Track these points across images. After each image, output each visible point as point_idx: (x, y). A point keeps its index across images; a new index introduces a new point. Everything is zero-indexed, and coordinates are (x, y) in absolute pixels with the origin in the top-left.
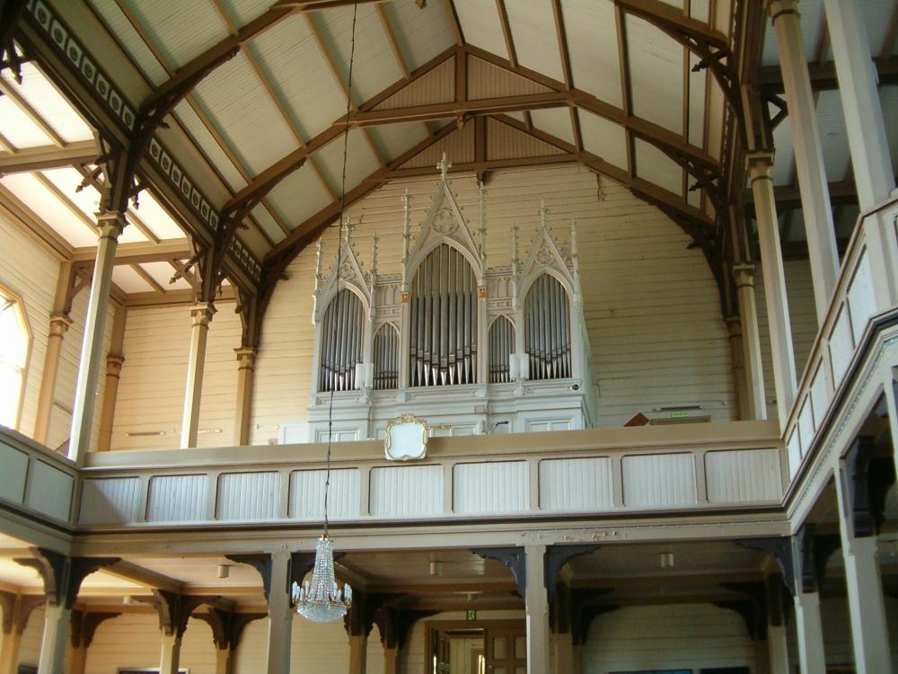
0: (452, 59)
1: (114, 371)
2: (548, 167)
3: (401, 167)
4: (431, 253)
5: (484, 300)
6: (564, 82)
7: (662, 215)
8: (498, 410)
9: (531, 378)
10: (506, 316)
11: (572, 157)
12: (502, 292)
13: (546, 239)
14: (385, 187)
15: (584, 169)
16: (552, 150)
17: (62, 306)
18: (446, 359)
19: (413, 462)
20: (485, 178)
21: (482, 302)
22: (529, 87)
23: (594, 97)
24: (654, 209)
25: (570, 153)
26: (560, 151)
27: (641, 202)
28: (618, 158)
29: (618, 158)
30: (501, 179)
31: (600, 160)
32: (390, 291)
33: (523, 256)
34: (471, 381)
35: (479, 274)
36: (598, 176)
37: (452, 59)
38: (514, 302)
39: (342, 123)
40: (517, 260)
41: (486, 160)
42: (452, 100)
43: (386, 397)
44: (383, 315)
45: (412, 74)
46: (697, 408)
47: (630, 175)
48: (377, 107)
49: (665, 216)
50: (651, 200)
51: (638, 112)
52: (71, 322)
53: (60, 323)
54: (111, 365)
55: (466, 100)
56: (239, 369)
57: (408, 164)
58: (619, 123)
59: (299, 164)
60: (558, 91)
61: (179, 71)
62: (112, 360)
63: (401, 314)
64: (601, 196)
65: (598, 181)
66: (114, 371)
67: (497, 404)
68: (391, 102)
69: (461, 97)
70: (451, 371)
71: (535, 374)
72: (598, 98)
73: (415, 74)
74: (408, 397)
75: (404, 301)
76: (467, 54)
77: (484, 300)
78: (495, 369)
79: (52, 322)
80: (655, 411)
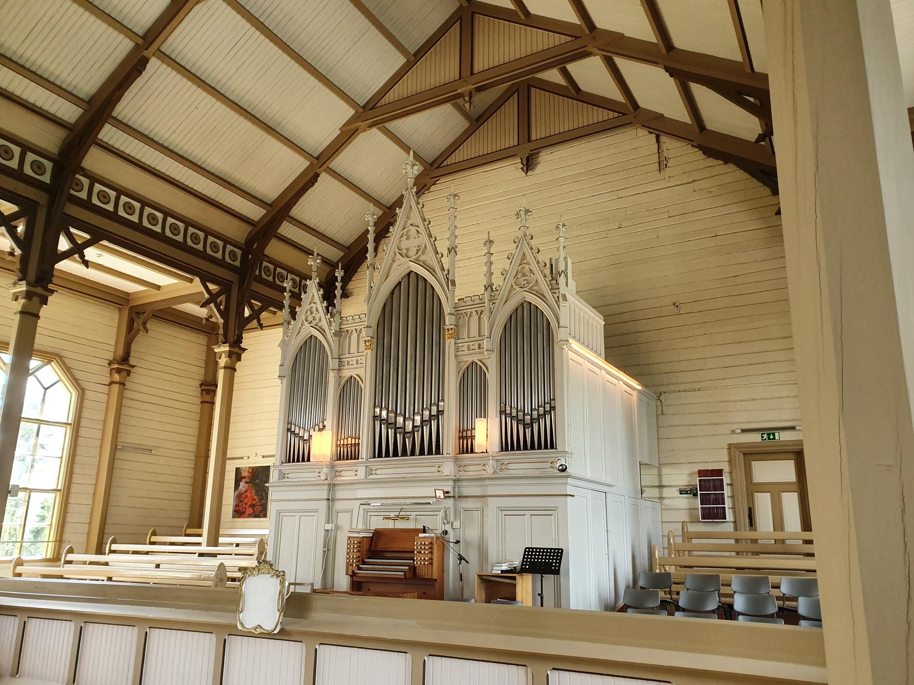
0: (458, 24)
1: (208, 398)
2: (561, 147)
3: (445, 163)
4: (400, 282)
5: (452, 341)
6: (656, 41)
7: (741, 175)
8: (466, 491)
9: (502, 450)
10: (479, 363)
11: (626, 119)
12: (474, 332)
13: (527, 254)
14: (433, 188)
15: (642, 132)
16: (603, 115)
17: (120, 352)
18: (436, 408)
19: (269, 636)
20: (529, 164)
21: (450, 343)
22: (543, 41)
23: (623, 34)
24: (731, 167)
25: (624, 114)
26: (612, 115)
27: (712, 162)
28: (678, 112)
29: (678, 112)
30: (548, 160)
31: (660, 117)
32: (355, 335)
33: (497, 281)
34: (438, 452)
35: (447, 309)
36: (658, 137)
37: (458, 24)
38: (486, 344)
39: (348, 128)
40: (491, 286)
41: (529, 141)
42: (457, 77)
43: (351, 472)
44: (346, 367)
45: (415, 55)
46: (793, 428)
47: (697, 130)
48: (383, 102)
49: (747, 176)
50: (727, 158)
51: (679, 42)
52: (133, 366)
53: (119, 371)
54: (204, 392)
55: (472, 74)
57: (452, 159)
58: (655, 63)
59: (316, 177)
61: (93, 99)
62: (204, 387)
63: (364, 365)
64: (662, 164)
65: (658, 141)
66: (208, 398)
67: (464, 484)
70: (426, 430)
71: (508, 445)
72: (627, 34)
73: (415, 58)
74: (369, 471)
75: (367, 348)
76: (473, 13)
77: (452, 341)
78: (465, 434)
79: (111, 370)
80: (733, 432)
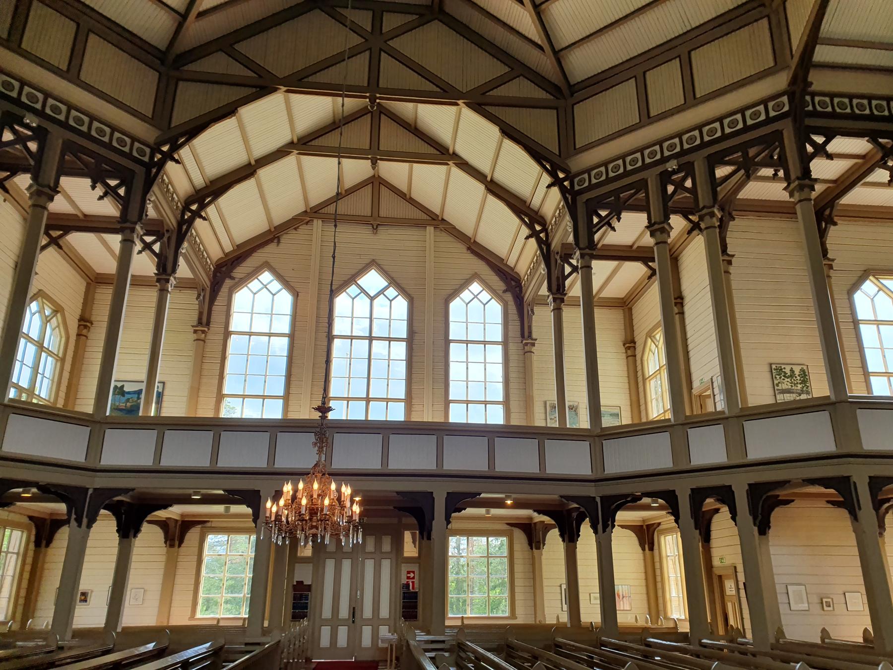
25: (434, 220)
56: (194, 341)
60: (434, 220)
68: (331, 209)
69: (376, 214)
